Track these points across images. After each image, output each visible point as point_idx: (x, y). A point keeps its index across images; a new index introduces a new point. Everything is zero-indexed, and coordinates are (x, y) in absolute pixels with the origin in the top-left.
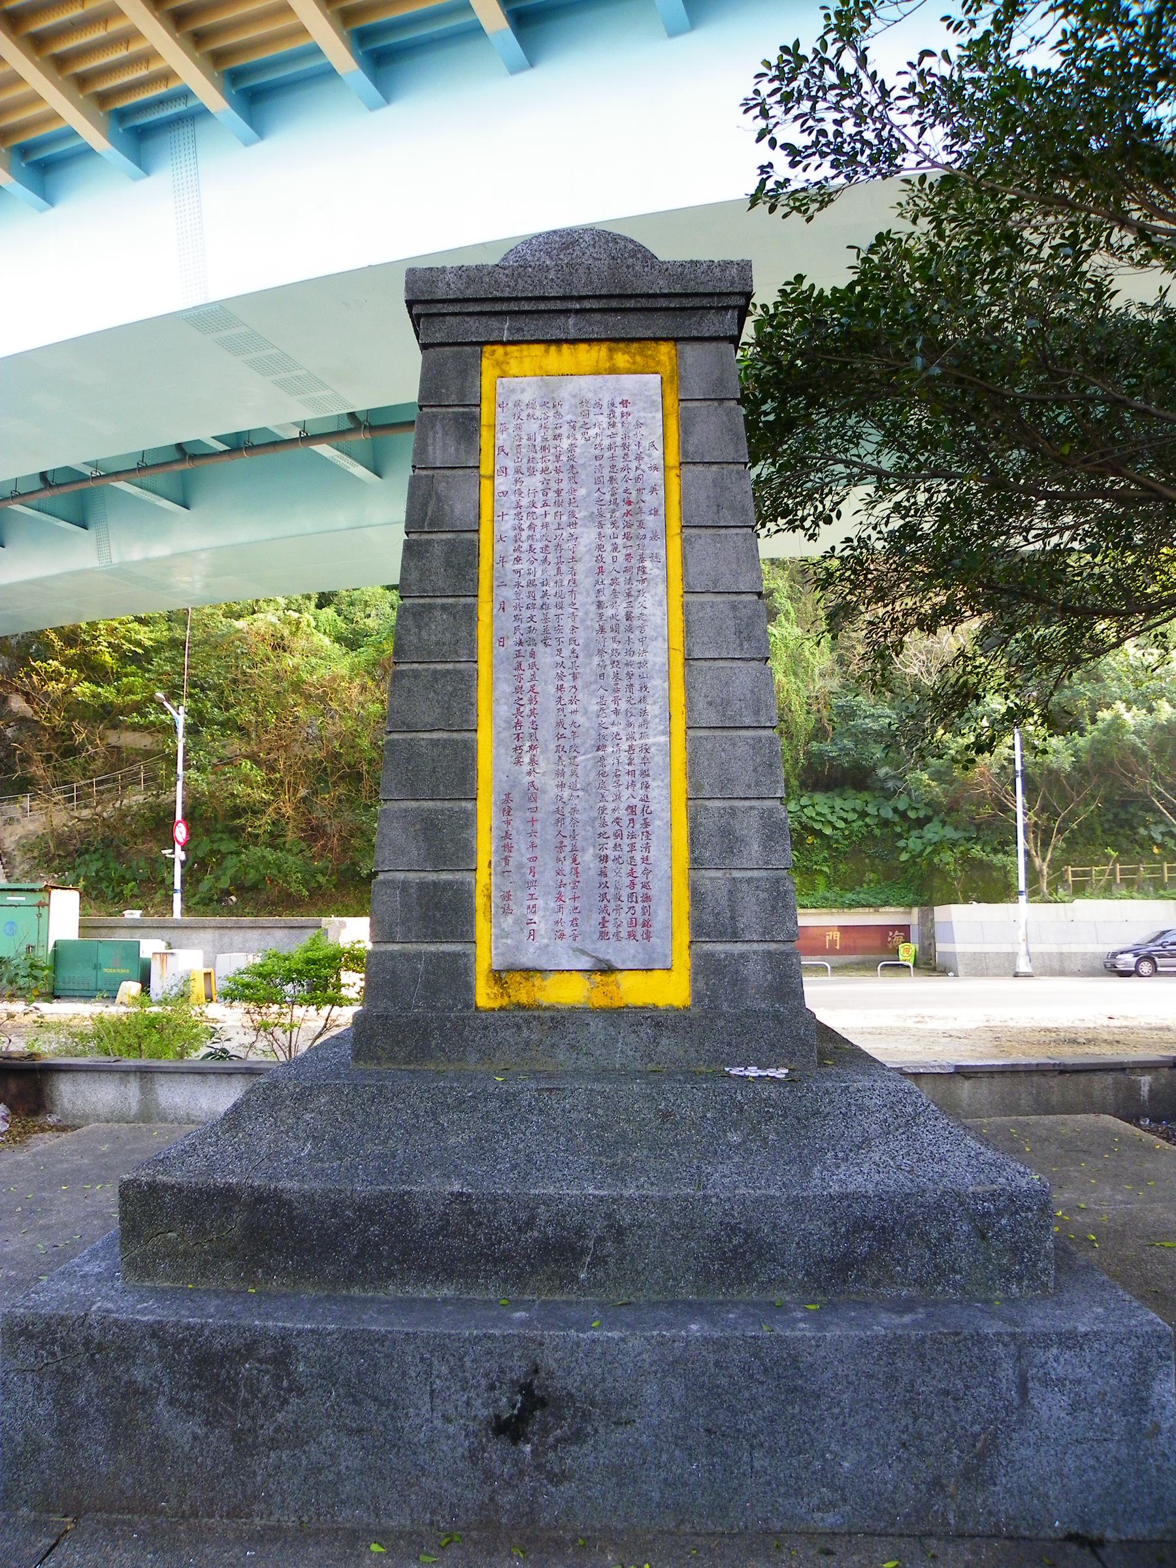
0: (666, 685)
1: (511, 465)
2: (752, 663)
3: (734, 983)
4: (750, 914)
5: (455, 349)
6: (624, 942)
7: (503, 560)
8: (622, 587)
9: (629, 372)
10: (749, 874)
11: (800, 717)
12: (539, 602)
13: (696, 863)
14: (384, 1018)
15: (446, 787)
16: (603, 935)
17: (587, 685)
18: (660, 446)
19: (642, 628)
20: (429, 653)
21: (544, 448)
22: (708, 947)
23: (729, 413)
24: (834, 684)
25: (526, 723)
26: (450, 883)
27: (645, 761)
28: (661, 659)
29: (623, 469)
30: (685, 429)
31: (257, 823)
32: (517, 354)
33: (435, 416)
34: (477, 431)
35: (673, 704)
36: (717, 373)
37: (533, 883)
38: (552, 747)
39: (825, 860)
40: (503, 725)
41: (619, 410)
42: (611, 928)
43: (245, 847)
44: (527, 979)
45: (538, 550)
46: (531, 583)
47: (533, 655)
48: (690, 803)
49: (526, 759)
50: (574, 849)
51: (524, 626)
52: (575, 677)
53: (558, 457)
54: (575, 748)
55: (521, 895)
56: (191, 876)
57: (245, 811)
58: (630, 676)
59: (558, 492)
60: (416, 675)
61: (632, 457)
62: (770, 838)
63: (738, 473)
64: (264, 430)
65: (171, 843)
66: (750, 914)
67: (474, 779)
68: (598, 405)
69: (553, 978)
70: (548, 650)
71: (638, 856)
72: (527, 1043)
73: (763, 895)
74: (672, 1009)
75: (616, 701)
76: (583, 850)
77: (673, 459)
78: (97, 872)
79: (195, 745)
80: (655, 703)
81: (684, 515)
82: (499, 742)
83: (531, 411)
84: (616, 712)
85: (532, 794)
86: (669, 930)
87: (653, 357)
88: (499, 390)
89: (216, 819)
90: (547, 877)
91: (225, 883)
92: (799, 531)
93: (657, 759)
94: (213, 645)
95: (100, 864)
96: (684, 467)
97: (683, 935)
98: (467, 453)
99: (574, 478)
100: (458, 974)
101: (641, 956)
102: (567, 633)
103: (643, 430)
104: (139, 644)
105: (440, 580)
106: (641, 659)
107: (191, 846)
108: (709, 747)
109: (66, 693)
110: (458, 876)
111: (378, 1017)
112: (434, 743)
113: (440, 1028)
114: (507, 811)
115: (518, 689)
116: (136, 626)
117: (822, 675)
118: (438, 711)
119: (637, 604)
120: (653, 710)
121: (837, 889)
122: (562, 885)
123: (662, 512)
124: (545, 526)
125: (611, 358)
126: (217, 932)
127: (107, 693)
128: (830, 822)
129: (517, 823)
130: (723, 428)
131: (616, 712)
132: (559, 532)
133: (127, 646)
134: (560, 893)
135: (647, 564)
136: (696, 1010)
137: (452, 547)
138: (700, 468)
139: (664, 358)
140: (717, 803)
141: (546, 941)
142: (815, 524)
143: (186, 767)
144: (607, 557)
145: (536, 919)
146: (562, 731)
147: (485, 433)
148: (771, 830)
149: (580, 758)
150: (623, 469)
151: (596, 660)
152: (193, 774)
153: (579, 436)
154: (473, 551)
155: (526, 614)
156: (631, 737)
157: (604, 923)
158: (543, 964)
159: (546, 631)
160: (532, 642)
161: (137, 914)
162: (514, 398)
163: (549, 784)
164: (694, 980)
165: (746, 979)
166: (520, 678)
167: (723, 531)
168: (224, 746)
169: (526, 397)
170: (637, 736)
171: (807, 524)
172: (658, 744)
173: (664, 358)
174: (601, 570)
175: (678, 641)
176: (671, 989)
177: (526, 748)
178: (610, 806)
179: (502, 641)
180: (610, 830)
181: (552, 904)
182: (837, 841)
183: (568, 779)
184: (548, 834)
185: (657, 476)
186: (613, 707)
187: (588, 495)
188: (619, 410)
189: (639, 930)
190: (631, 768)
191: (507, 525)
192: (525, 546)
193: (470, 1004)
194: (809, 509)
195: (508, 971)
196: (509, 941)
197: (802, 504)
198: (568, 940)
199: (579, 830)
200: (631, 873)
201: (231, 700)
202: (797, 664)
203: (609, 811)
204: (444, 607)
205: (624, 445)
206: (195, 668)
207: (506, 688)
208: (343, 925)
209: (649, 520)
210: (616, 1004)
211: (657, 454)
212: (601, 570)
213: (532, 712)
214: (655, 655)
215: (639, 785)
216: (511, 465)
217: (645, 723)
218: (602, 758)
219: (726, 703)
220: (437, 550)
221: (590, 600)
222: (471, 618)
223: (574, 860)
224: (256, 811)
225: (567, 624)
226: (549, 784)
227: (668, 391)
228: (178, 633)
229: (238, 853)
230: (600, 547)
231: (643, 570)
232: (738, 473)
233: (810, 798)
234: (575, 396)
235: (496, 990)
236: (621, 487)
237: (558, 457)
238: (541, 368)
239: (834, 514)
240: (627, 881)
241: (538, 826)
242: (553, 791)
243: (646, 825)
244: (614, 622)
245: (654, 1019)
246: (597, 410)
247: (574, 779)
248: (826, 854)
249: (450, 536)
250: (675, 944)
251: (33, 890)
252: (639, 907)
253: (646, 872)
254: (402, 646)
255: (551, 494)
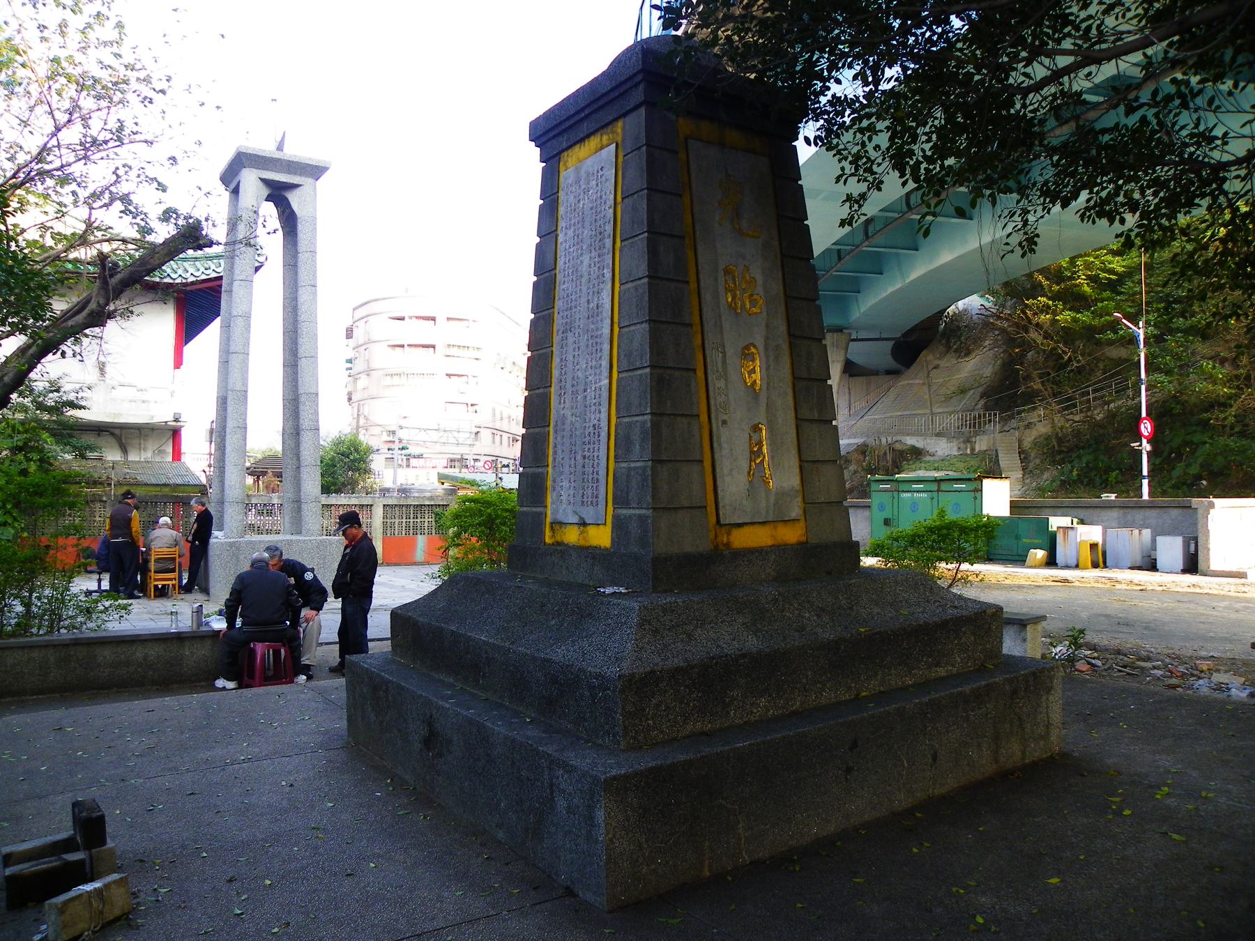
65: (1138, 436)
78: (1087, 464)
91: (1194, 470)
95: (1091, 457)
104: (1112, 271)
109: (1054, 322)
110: (540, 470)
116: (1109, 258)
126: (1121, 511)
127: (1085, 317)
133: (1103, 275)
161: (1113, 497)
208: (1212, 506)
224: (1223, 404)
251: (969, 480)
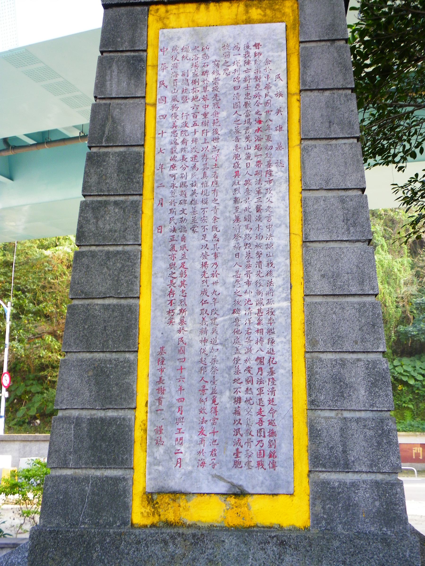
0: (288, 262)
1: (169, 95)
2: (358, 244)
3: (347, 508)
4: (359, 448)
5: (129, 8)
6: (254, 470)
7: (162, 167)
8: (254, 186)
9: (261, 22)
10: (358, 415)
11: (392, 310)
12: (189, 199)
13: (313, 404)
14: (55, 533)
15: (114, 342)
16: (237, 464)
17: (225, 262)
18: (284, 77)
19: (269, 218)
20: (104, 238)
21: (194, 82)
22: (323, 476)
23: (339, 50)
24: (414, 289)
25: (178, 292)
26: (114, 419)
27: (271, 322)
28: (284, 242)
29: (255, 96)
30: (304, 64)
31: (55, 374)
32: (175, 11)
33: (112, 59)
34: (144, 70)
35: (294, 277)
36: (330, 19)
37: (180, 420)
38: (197, 310)
39: (411, 400)
40: (160, 293)
41: (253, 51)
42: (243, 458)
43: (47, 389)
44: (174, 500)
45: (189, 159)
46: (183, 185)
47: (183, 239)
48: (308, 355)
49: (177, 320)
50: (214, 392)
51: (177, 217)
52: (216, 256)
53: (205, 89)
54: (214, 311)
55: (170, 429)
56: (12, 407)
57: (47, 366)
58: (259, 255)
59: (205, 115)
60: (93, 255)
61: (262, 87)
62: (374, 384)
63: (346, 96)
64: (56, 131)
66: (359, 448)
67: (136, 336)
68: (237, 48)
69: (196, 500)
70: (196, 235)
71: (265, 398)
72: (173, 557)
73: (370, 433)
74: (294, 529)
75: (248, 274)
76: (221, 393)
77: (295, 87)
79: (17, 325)
80: (279, 276)
81: (302, 130)
82: (156, 307)
83: (185, 54)
84: (248, 283)
85: (181, 347)
86: (291, 461)
87: (279, 10)
88: (161, 38)
89: (29, 372)
90: (192, 414)
91: (33, 412)
92: (392, 166)
93: (281, 320)
94: (29, 264)
96: (303, 94)
97: (303, 465)
98: (136, 86)
99: (217, 105)
100: (116, 495)
101: (267, 483)
102: (210, 222)
103: (271, 66)
105: (114, 182)
106: (268, 242)
107: (13, 389)
108: (323, 310)
110: (121, 413)
111: (50, 532)
112: (106, 307)
113: (101, 542)
114: (161, 361)
115: (172, 266)
117: (406, 284)
118: (109, 282)
119: (265, 200)
120: (277, 281)
121: (418, 419)
122: (204, 421)
123: (285, 128)
124: (195, 140)
125: (247, 12)
126: (22, 444)
128: (413, 377)
129: (169, 370)
130: (334, 67)
131: (248, 283)
132: (205, 145)
134: (202, 428)
135: (274, 168)
136: (314, 531)
137: (123, 157)
138: (316, 93)
139: (288, 10)
140: (330, 356)
141: (190, 468)
142: (404, 159)
143: (12, 339)
144: (242, 164)
145: (182, 449)
146: (205, 298)
147: (150, 71)
148: (375, 379)
149: (219, 320)
150: (255, 96)
151: (233, 243)
152: (15, 344)
153: (221, 72)
154: (139, 161)
155: (179, 208)
156: (260, 303)
157: (237, 453)
158: (187, 487)
159: (194, 220)
160: (183, 229)
162: (172, 44)
163: (194, 339)
164: (313, 505)
165: (356, 505)
166: (173, 257)
167: (334, 142)
168: (36, 327)
169: (182, 44)
170: (265, 302)
171: (397, 159)
172: (282, 309)
173: (288, 10)
174: (237, 174)
175: (297, 228)
176: (293, 511)
177: (177, 311)
178: (243, 357)
179: (160, 228)
180: (243, 376)
181: (196, 438)
182: (418, 389)
183: (209, 336)
184: (193, 379)
185: (282, 100)
186: (245, 279)
187: (228, 117)
188: (253, 51)
189: (267, 460)
190: (259, 327)
191: (166, 140)
192: (179, 156)
193: (126, 521)
194: (399, 148)
195: (159, 493)
196: (160, 468)
197: (394, 144)
198: (208, 468)
199: (218, 377)
200: (260, 412)
201: (41, 298)
202: (389, 275)
203: (242, 362)
204: (116, 203)
205: (256, 78)
206: (19, 279)
207: (163, 265)
209: (276, 135)
210: (248, 523)
211: (282, 84)
212: (237, 174)
213: (183, 283)
214: (279, 239)
215: (266, 341)
216: (169, 95)
217: (271, 292)
218: (237, 320)
219: (336, 276)
220: (112, 160)
221: (228, 197)
222: (137, 211)
223: (214, 401)
225: (210, 215)
226: (194, 339)
227: (291, 36)
228: (9, 258)
229: (42, 393)
230: (237, 156)
231: (270, 173)
232: (346, 96)
233: (400, 361)
234: (219, 41)
235: (149, 509)
236: (253, 109)
237: (205, 89)
238: (193, 21)
239: (417, 151)
240: (256, 418)
241: (185, 373)
242: (197, 345)
243: (272, 372)
244: (247, 213)
245: (279, 538)
246: (236, 52)
247: (214, 335)
248: (411, 396)
249: (122, 149)
250: (297, 472)
252: (266, 441)
253: (272, 411)
254: (83, 233)
255: (200, 117)
